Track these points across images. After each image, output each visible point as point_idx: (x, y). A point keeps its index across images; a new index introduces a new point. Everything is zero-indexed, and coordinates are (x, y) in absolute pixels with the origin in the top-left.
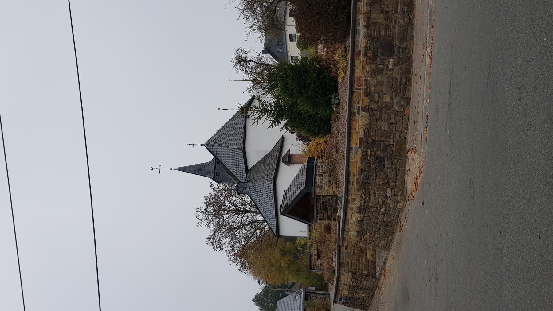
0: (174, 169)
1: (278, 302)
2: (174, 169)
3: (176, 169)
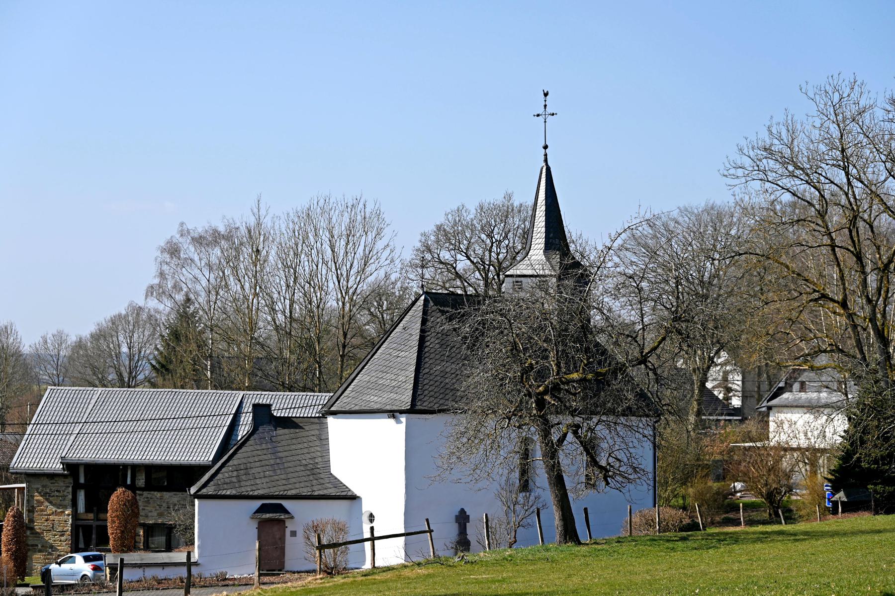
0: (546, 155)
1: (334, 471)
2: (546, 155)
3: (546, 161)
